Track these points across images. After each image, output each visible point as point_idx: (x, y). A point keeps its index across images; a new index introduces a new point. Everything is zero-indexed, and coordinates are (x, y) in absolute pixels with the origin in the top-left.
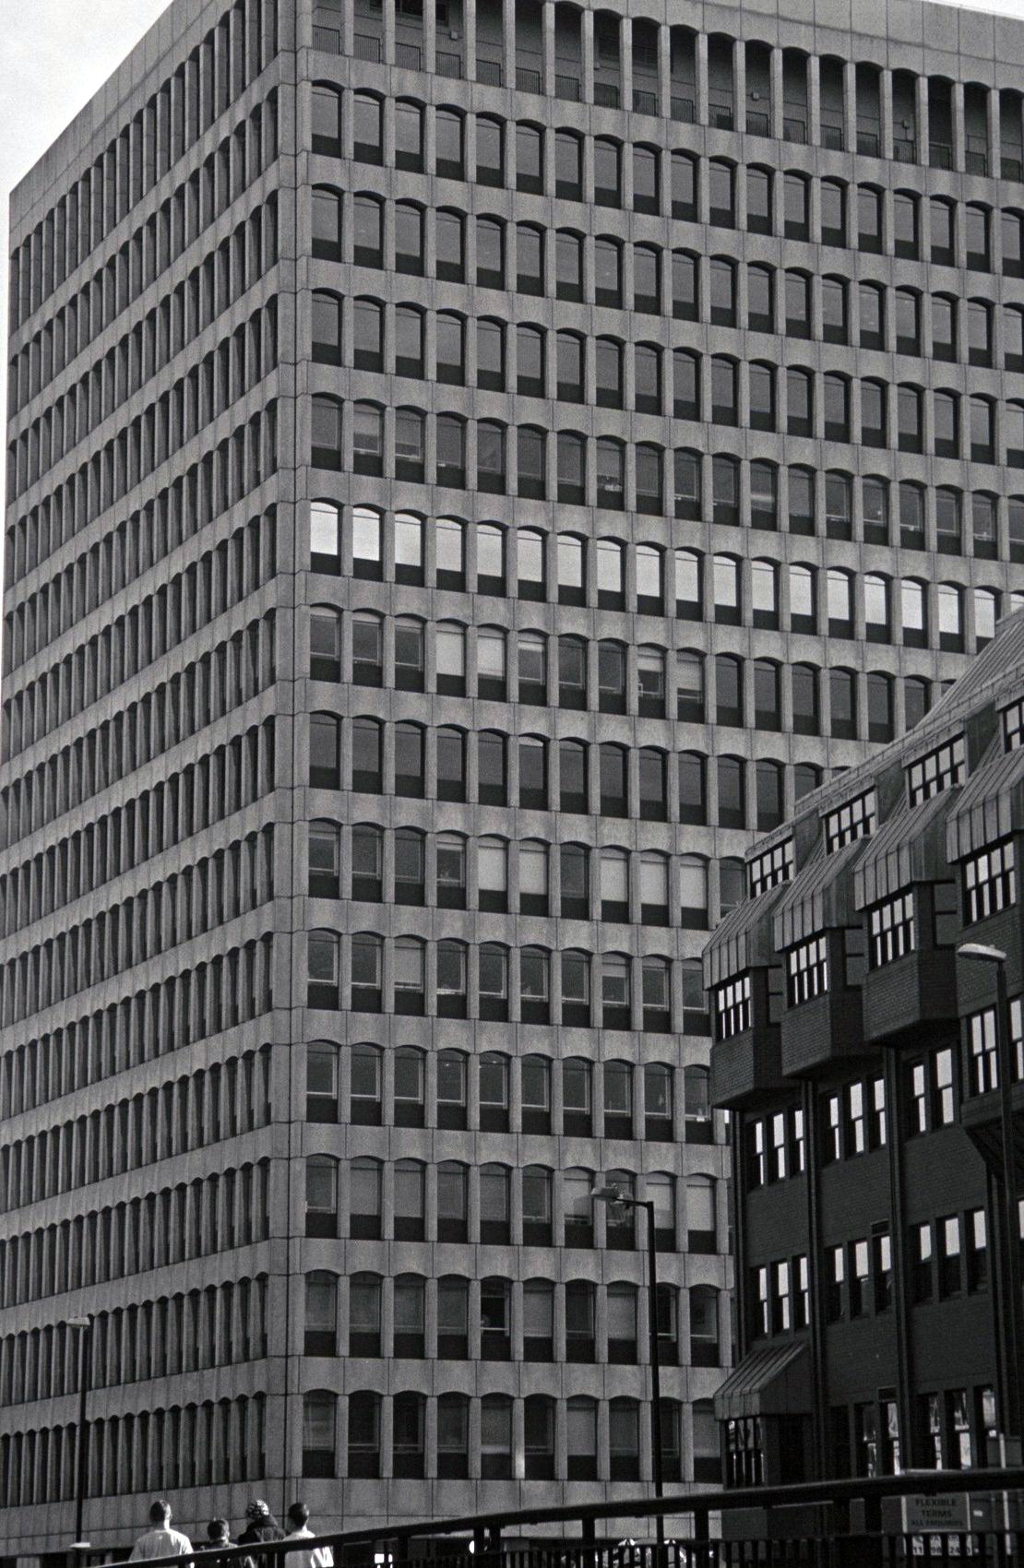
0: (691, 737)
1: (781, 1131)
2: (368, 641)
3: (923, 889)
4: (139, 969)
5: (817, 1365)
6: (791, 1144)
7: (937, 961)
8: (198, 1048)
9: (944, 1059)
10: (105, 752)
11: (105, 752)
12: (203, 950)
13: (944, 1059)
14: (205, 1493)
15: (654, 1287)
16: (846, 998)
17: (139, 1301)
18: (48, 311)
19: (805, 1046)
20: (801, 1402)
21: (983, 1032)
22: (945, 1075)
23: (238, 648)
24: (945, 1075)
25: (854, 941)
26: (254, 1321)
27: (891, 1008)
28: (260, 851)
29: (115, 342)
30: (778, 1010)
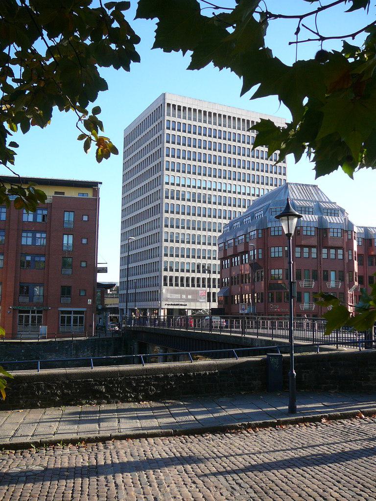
0: (214, 207)
1: (226, 262)
2: (172, 236)
3: (245, 235)
4: (141, 235)
5: (230, 290)
6: (228, 264)
7: (246, 244)
8: (149, 246)
9: (247, 255)
10: (139, 144)
11: (139, 144)
12: (150, 233)
13: (247, 255)
14: (150, 302)
15: (210, 287)
16: (235, 247)
17: (141, 278)
18: (129, 146)
19: (230, 252)
20: (228, 294)
21: (251, 253)
22: (247, 257)
23: (155, 194)
24: (247, 257)
25: (236, 240)
26: (157, 252)
27: (241, 249)
28: (157, 249)
29: (138, 164)
30: (227, 248)
